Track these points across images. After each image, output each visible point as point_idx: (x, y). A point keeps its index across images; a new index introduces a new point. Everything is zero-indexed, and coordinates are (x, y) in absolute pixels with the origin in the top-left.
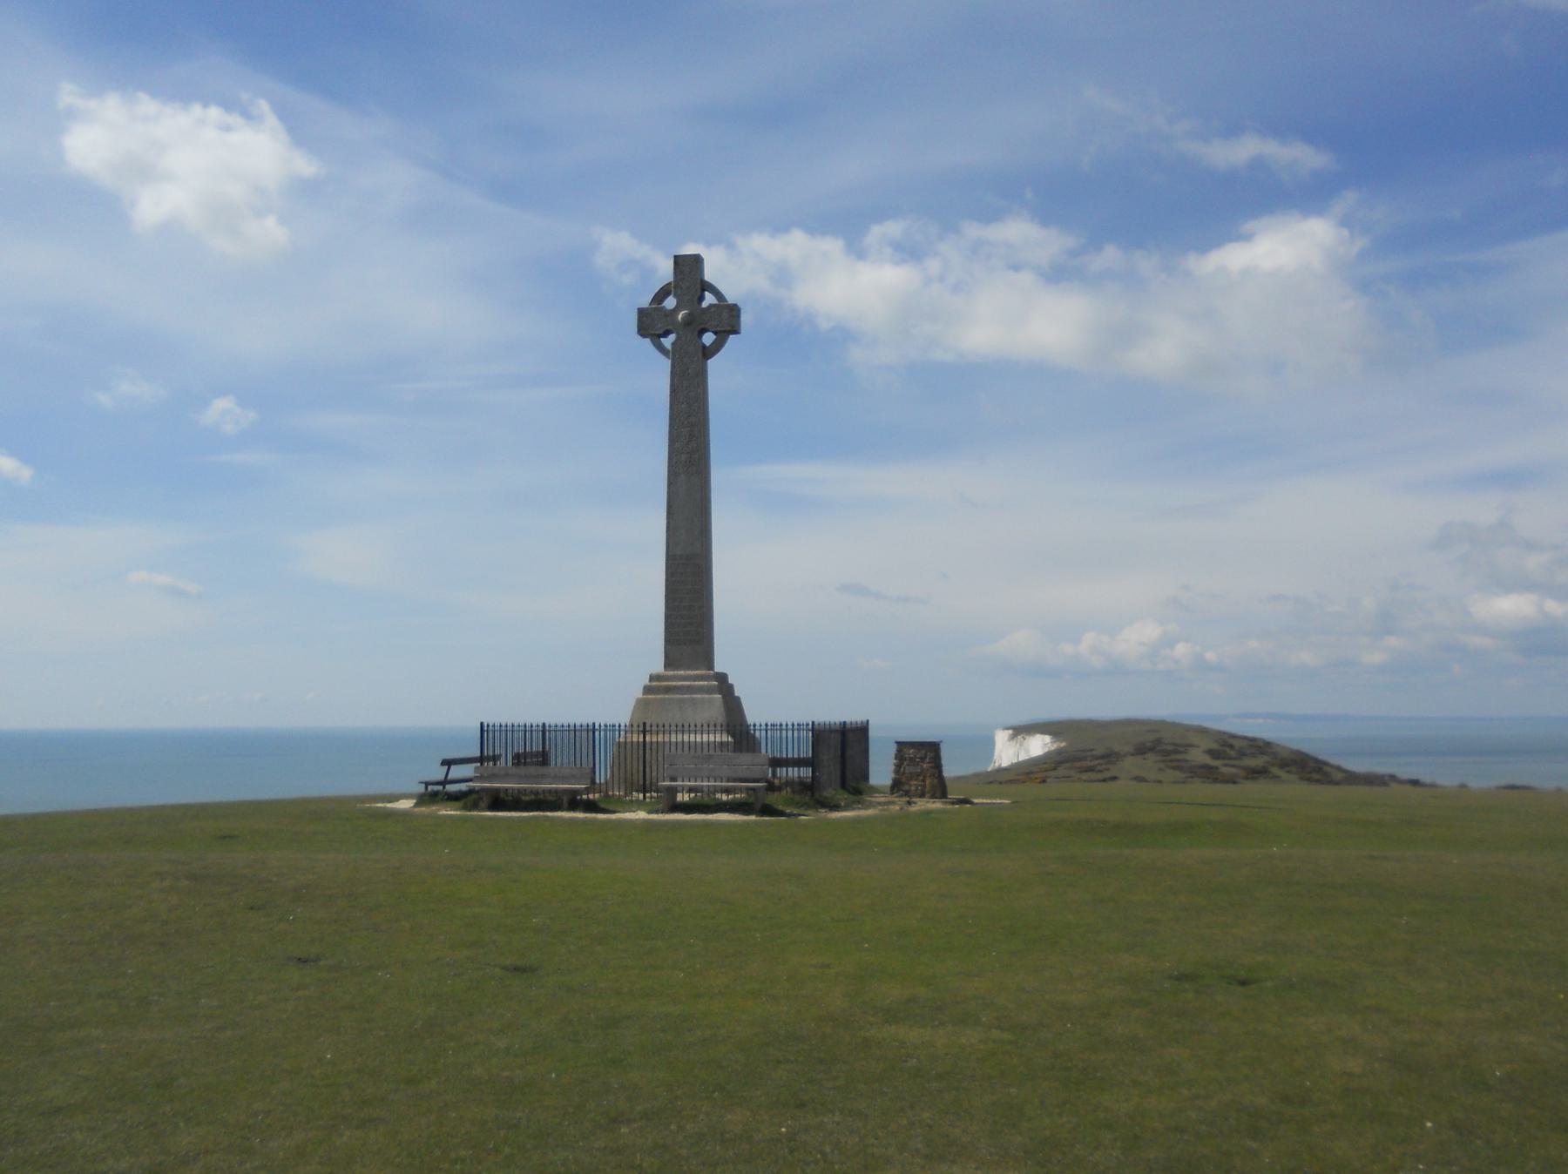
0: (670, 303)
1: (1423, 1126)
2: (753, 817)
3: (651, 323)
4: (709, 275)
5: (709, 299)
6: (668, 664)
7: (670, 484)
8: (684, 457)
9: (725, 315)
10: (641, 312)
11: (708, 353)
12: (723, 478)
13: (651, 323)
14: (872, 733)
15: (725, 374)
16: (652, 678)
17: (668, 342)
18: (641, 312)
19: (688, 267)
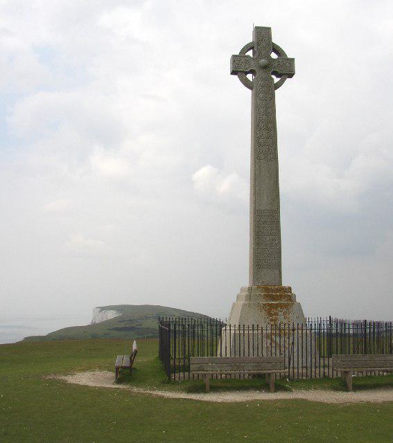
3: (239, 67)
4: (276, 39)
13: (239, 67)
19: (262, 34)
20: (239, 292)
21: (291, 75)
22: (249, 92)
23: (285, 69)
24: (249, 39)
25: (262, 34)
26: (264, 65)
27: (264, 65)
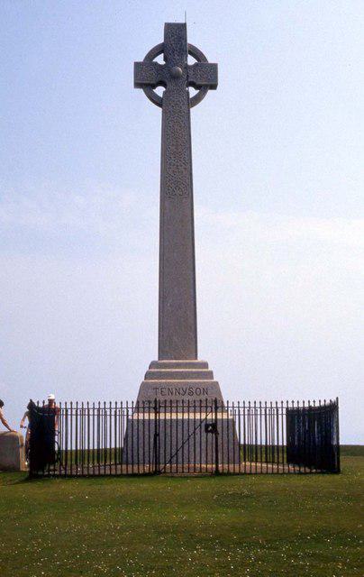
3: (147, 77)
4: (192, 39)
13: (147, 77)
19: (176, 34)
20: (146, 368)
21: (214, 87)
22: (159, 110)
23: (206, 78)
24: (159, 39)
25: (176, 34)
27: (175, 74)
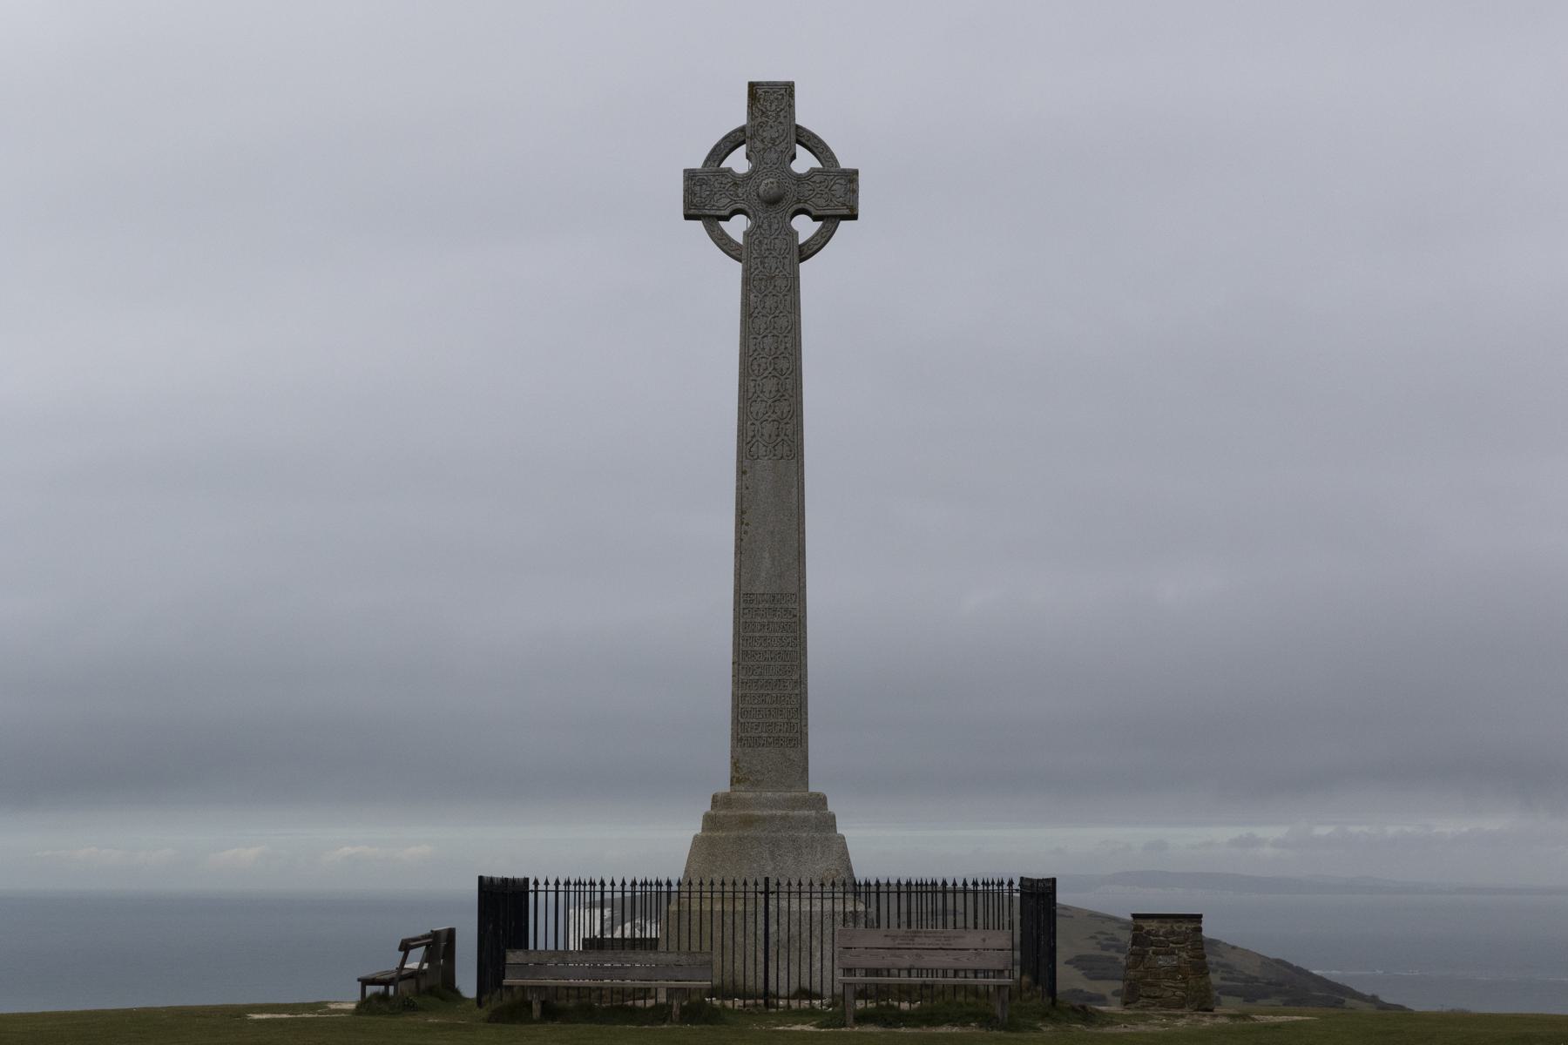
0: (738, 162)
1: (396, 990)
2: (955, 1030)
3: (705, 197)
4: (805, 115)
5: (804, 162)
6: (735, 781)
7: (741, 472)
8: (768, 428)
9: (838, 189)
10: (690, 175)
11: (807, 251)
12: (698, 608)
13: (705, 197)
14: (1062, 898)
15: (835, 283)
16: (715, 800)
17: (737, 227)
18: (690, 175)
19: (772, 101)
23: (835, 198)
24: (737, 115)
25: (772, 101)
26: (772, 191)
